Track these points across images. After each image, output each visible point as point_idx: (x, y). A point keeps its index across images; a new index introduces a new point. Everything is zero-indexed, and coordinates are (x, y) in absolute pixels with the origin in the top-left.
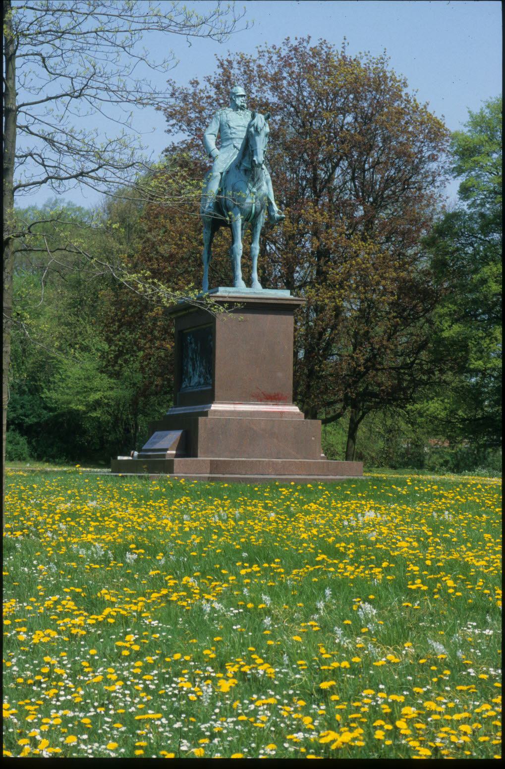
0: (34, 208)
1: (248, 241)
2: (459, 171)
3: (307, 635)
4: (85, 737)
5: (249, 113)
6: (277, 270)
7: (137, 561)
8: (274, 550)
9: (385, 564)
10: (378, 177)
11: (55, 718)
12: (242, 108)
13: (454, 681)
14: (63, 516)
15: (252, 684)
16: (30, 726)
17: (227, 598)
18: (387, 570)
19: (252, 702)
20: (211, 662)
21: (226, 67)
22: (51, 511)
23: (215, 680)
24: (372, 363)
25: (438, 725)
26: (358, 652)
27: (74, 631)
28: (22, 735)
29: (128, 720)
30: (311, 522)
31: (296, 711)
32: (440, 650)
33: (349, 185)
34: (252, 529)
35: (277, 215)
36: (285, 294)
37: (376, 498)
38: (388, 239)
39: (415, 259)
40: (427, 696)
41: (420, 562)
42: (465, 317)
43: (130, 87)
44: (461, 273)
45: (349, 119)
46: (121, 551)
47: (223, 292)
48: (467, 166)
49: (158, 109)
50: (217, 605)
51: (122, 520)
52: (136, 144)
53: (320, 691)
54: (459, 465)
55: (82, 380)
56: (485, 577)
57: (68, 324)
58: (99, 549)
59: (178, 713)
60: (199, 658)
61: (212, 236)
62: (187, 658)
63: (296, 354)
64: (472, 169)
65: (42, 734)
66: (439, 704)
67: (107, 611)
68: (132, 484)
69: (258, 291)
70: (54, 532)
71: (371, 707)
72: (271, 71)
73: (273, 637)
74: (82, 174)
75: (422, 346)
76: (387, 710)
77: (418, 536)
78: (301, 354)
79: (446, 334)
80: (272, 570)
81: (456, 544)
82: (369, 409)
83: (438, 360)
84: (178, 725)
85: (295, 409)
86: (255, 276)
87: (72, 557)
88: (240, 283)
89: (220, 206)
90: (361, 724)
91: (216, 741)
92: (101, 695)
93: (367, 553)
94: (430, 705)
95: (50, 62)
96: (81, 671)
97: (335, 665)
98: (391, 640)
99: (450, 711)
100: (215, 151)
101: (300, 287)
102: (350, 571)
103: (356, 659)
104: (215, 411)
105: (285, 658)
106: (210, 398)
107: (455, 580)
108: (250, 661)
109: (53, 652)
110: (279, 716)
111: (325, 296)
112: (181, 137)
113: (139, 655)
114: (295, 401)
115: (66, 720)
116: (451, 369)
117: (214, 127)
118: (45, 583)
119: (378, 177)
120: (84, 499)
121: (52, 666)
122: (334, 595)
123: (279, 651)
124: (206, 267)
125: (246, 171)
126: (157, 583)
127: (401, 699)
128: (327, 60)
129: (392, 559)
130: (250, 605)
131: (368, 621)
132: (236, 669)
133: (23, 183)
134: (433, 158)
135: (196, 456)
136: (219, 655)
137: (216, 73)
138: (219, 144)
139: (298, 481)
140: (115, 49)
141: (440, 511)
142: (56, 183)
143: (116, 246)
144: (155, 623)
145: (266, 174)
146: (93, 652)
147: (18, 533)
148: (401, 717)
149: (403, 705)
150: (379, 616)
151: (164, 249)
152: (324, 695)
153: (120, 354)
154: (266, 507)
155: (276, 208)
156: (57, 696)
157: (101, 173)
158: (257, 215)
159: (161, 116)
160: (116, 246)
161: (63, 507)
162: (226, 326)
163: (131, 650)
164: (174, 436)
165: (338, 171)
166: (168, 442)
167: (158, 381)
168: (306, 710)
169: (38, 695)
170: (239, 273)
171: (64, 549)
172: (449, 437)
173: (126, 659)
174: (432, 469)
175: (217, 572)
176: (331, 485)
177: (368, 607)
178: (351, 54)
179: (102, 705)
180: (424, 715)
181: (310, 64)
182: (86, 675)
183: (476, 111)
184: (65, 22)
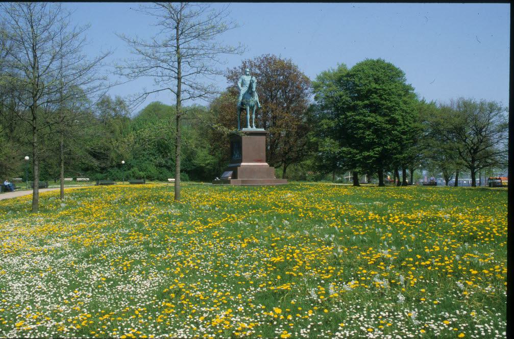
0: (189, 106)
1: (251, 114)
2: (314, 92)
3: (268, 230)
4: (203, 260)
5: (250, 77)
6: (261, 123)
7: (219, 210)
8: (259, 205)
9: (292, 209)
10: (290, 94)
11: (194, 255)
12: (248, 75)
13: (311, 242)
14: (198, 197)
15: (252, 245)
16: (187, 257)
17: (245, 220)
18: (293, 211)
19: (252, 250)
20: (240, 239)
21: (244, 64)
22: (194, 196)
23: (241, 244)
24: (290, 149)
25: (306, 254)
26: (283, 234)
27: (200, 230)
28: (185, 260)
29: (215, 255)
30: (272, 197)
31: (264, 252)
32: (307, 233)
33: (282, 97)
34: (254, 200)
35: (260, 106)
36: (263, 130)
37: (291, 189)
38: (294, 113)
39: (302, 118)
40: (303, 247)
41: (303, 208)
42: (317, 135)
43: (214, 69)
44: (316, 122)
45: (281, 77)
46: (214, 207)
47: (244, 129)
48: (317, 90)
49: (224, 76)
50: (242, 222)
51: (215, 198)
52: (216, 86)
53: (272, 246)
54: (317, 179)
55: (204, 157)
56: (321, 212)
57: (199, 141)
58: (208, 206)
59: (230, 253)
60: (236, 238)
61: (241, 113)
62: (233, 238)
63: (267, 148)
64: (318, 92)
65: (191, 259)
66: (306, 249)
67: (209, 224)
68: (218, 187)
69: (254, 129)
70: (195, 202)
71: (287, 250)
72: (258, 64)
73: (258, 231)
74: (200, 96)
75: (304, 145)
76: (291, 251)
77: (303, 200)
78: (269, 148)
79: (311, 141)
80: (259, 212)
81: (314, 203)
82: (289, 163)
83: (309, 148)
84: (230, 257)
85: (267, 164)
86: (254, 124)
87: (200, 209)
88: (249, 127)
89: (242, 104)
90: (283, 255)
91: (241, 261)
92: (208, 248)
93: (288, 206)
94: (303, 249)
95: (190, 63)
96: (202, 242)
97: (276, 239)
98: (293, 231)
99: (309, 251)
100: (241, 88)
101: (268, 128)
102: (281, 211)
103: (283, 237)
104: (242, 165)
105: (261, 237)
106: (241, 161)
107: (312, 213)
108: (251, 238)
109: (194, 236)
110: (259, 253)
111: (276, 130)
112: (232, 84)
113: (219, 237)
114: (267, 162)
115: (197, 256)
116: (313, 151)
117: (240, 81)
118: (192, 217)
119: (290, 94)
120: (204, 192)
121: (193, 241)
122: (277, 219)
123: (260, 235)
124: (239, 122)
125: (250, 93)
126: (225, 216)
127: (295, 248)
128: (275, 60)
129: (294, 208)
130: (252, 222)
131: (287, 225)
132: (247, 240)
133: (103, 56)
134: (307, 89)
135: (237, 178)
136: (242, 237)
137: (241, 65)
138: (242, 86)
139: (268, 186)
140: (209, 59)
141: (310, 193)
142: (193, 98)
143: (213, 117)
144: (224, 228)
145: (256, 94)
146: (205, 236)
147: (184, 202)
148: (295, 253)
149: (296, 249)
150: (290, 224)
151: (228, 117)
152: (273, 247)
153: (214, 149)
154: (258, 193)
155: (259, 104)
156: (195, 249)
157: (206, 95)
158: (254, 106)
159: (225, 78)
160: (213, 117)
161: (198, 195)
162: (245, 140)
163: (216, 236)
164: (230, 173)
165: (279, 93)
166: (229, 175)
167: (226, 157)
168: (267, 252)
169: (190, 248)
170: (249, 124)
171: (197, 207)
172: (314, 171)
173: (216, 238)
174: (309, 181)
175: (242, 213)
176: (277, 186)
177: (286, 221)
178: (282, 59)
179: (208, 252)
180: (302, 252)
181: (269, 61)
182: (203, 243)
183: (319, 74)
184: (194, 52)
